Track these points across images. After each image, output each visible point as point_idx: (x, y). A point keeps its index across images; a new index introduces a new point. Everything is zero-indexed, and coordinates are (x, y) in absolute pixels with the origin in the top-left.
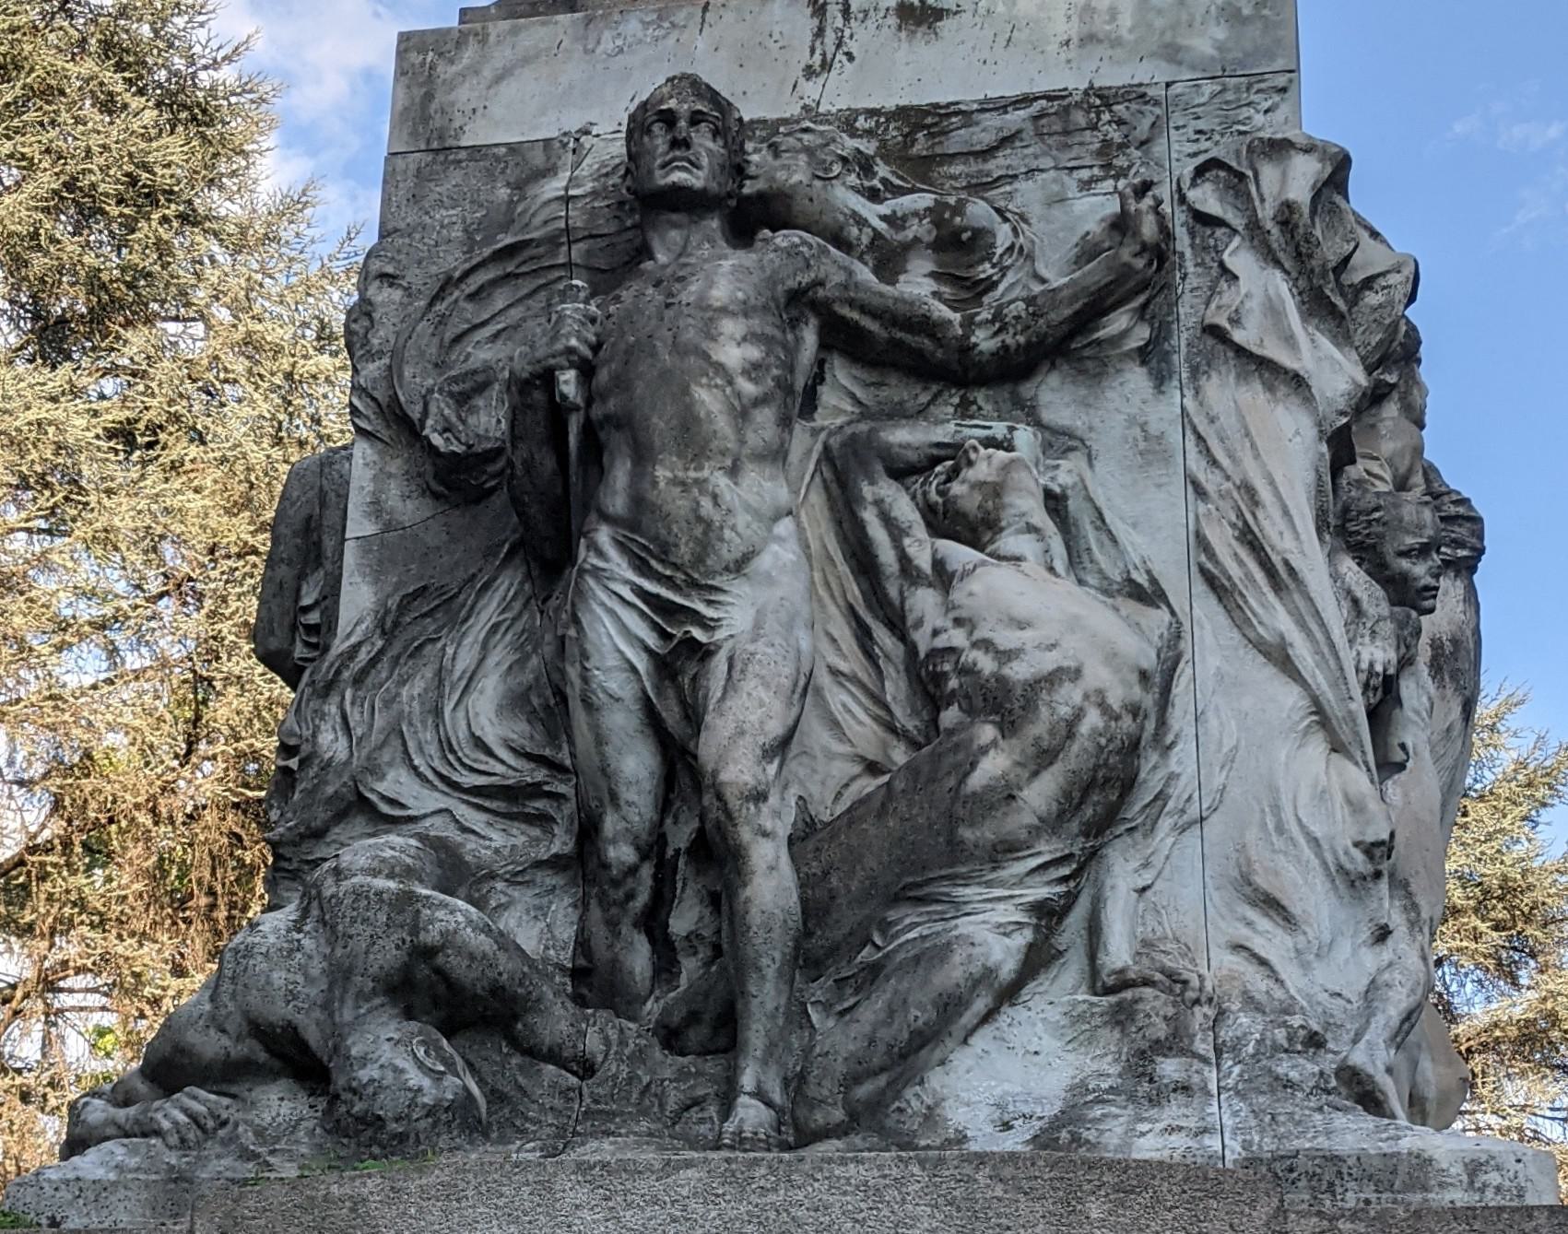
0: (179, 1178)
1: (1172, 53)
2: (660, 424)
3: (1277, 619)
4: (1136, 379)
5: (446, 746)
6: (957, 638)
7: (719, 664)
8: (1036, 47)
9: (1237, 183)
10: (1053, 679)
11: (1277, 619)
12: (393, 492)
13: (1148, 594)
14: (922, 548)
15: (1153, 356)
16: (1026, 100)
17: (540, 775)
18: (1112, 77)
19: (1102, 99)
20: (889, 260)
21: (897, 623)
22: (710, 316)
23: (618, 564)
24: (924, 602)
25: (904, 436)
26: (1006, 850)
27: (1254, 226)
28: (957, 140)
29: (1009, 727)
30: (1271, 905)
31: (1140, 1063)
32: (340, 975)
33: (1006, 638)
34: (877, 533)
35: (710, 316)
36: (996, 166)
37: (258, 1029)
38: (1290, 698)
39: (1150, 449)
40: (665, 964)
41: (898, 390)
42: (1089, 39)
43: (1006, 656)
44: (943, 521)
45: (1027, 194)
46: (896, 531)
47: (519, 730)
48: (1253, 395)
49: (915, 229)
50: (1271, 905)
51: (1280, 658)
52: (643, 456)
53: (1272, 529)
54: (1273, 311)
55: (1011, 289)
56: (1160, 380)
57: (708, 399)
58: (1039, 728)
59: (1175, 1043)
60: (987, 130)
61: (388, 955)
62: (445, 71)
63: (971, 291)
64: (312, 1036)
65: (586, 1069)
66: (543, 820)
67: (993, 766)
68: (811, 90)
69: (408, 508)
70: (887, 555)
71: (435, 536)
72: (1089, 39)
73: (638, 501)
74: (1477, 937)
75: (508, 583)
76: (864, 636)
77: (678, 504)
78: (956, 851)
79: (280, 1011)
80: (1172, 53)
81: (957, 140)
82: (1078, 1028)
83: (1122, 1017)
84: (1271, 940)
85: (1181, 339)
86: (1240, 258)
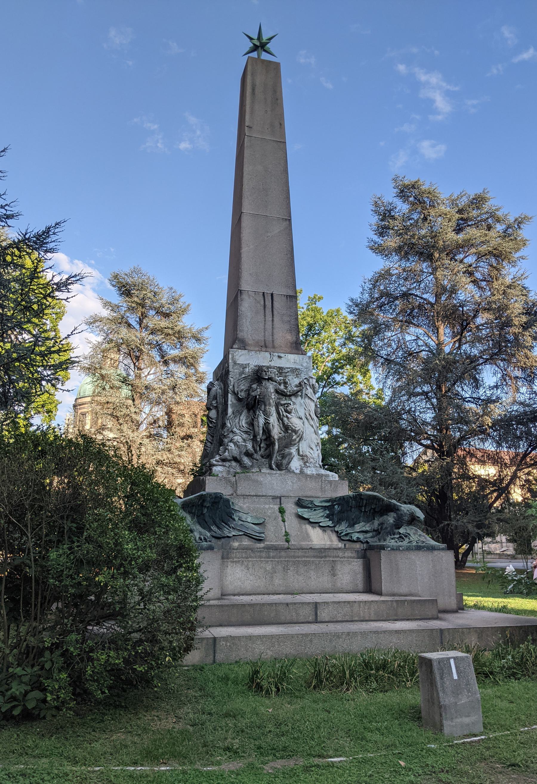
0: (229, 471)
1: (302, 365)
2: (267, 403)
3: (312, 423)
4: (300, 398)
5: (240, 426)
6: (291, 425)
7: (271, 424)
8: (290, 362)
9: (308, 380)
10: (299, 430)
11: (312, 423)
12: (233, 400)
13: (301, 418)
14: (285, 414)
15: (301, 396)
16: (290, 368)
17: (249, 430)
18: (297, 367)
19: (297, 369)
20: (280, 384)
21: (282, 420)
22: (271, 393)
23: (262, 415)
24: (285, 419)
25: (282, 402)
26: (295, 444)
27: (310, 385)
28: (284, 371)
29: (296, 434)
30: (312, 448)
31: (305, 463)
32: (241, 452)
33: (295, 426)
34: (281, 411)
35: (271, 393)
36: (287, 374)
37: (233, 457)
38: (313, 430)
39: (301, 405)
40: (260, 450)
41: (281, 397)
42: (295, 362)
43: (295, 427)
44: (286, 411)
45: (290, 378)
46: (282, 412)
47: (247, 425)
48: (309, 401)
49: (282, 381)
50: (312, 448)
51: (312, 427)
52: (265, 406)
53: (311, 414)
54: (311, 393)
55: (289, 388)
56: (302, 398)
57: (271, 401)
58: (298, 434)
59: (307, 462)
60: (286, 370)
61: (244, 451)
62: (235, 354)
63: (286, 387)
64: (238, 458)
65: (257, 460)
66: (249, 435)
67: (294, 437)
68: (270, 363)
69: (235, 402)
70: (281, 414)
71: (237, 405)
72: (295, 362)
73: (265, 410)
74: (174, 340)
75: (245, 411)
76: (279, 421)
77: (268, 410)
78: (291, 444)
79: (236, 455)
80: (302, 365)
81: (284, 371)
82: (299, 460)
83: (303, 459)
84: (311, 451)
85: (303, 394)
86: (308, 388)
